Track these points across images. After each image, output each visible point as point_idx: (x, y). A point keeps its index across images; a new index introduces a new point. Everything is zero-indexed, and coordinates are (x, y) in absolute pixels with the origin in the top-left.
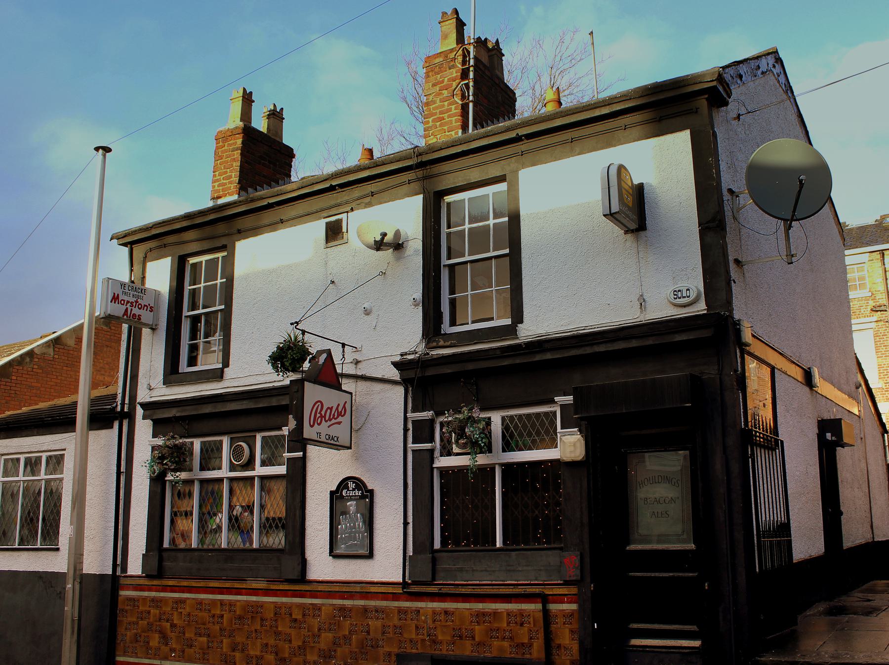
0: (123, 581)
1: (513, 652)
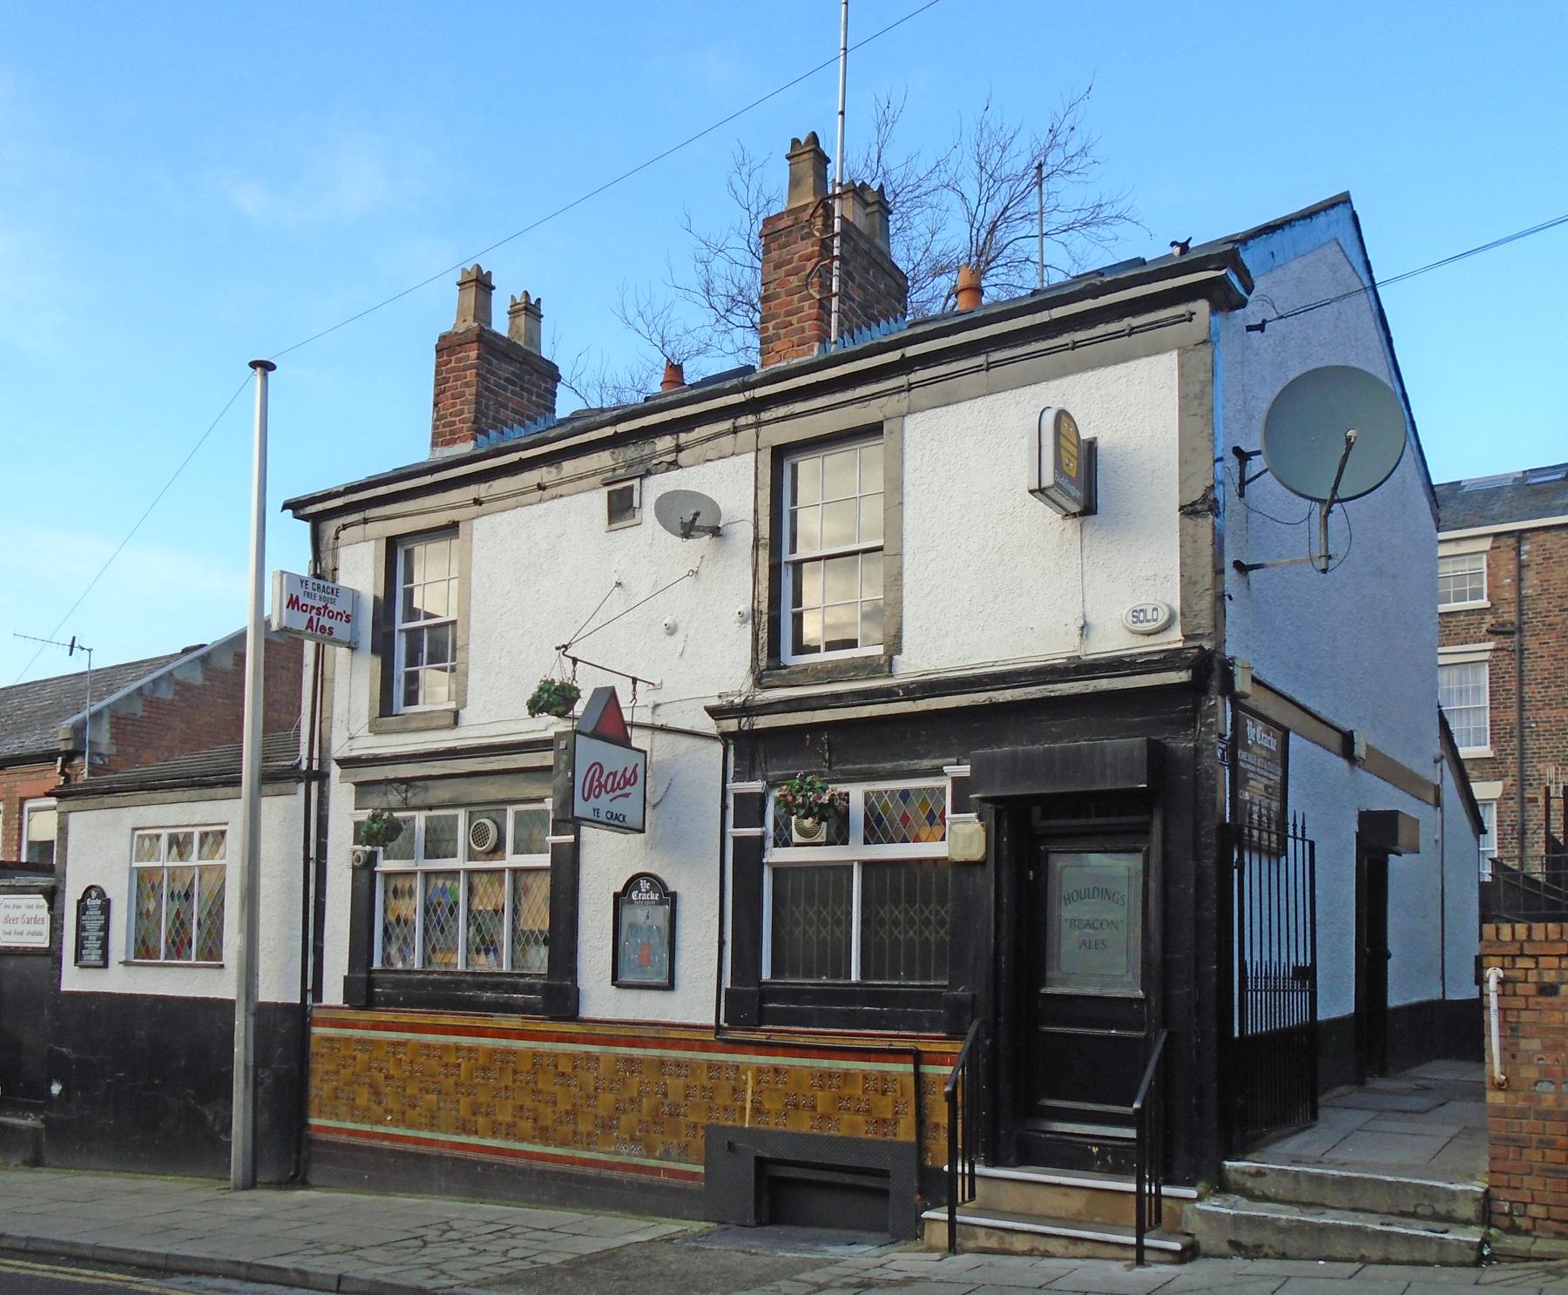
0: (317, 1014)
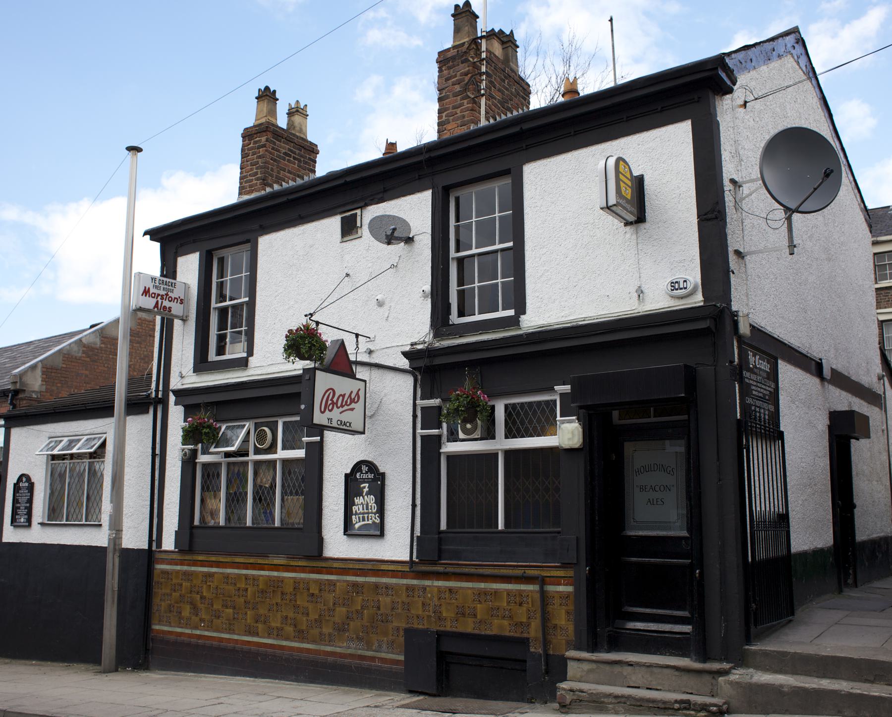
0: (158, 556)
1: (511, 631)
